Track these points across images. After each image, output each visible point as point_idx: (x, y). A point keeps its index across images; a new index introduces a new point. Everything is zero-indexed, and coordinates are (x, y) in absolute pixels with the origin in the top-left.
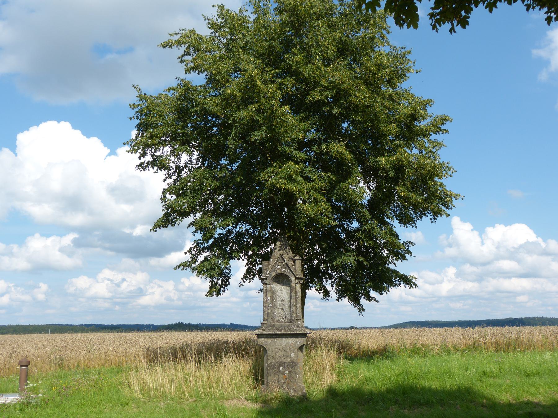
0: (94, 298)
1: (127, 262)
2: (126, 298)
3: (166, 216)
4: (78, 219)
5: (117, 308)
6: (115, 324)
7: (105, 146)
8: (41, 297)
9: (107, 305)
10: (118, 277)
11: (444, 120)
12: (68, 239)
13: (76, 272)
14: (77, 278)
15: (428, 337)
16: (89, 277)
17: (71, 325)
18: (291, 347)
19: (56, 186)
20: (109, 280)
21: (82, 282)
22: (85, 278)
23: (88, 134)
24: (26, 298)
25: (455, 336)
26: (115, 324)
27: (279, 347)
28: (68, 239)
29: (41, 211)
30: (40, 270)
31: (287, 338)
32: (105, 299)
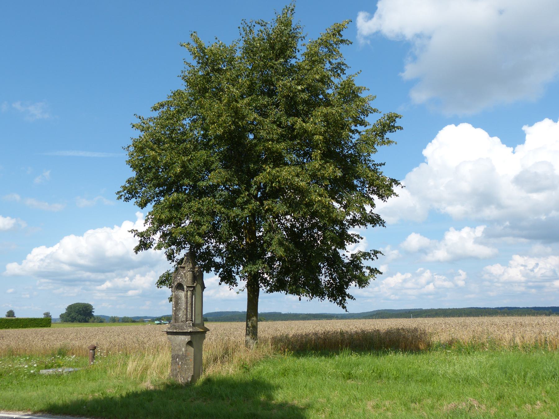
0: (510, 283)
1: (538, 247)
2: (539, 282)
3: (140, 245)
4: (490, 212)
5: (533, 291)
6: (547, 306)
7: (503, 143)
8: (461, 283)
9: (522, 289)
10: (531, 263)
11: (392, 118)
12: (480, 230)
13: (491, 260)
14: (492, 265)
15: (503, 329)
16: (502, 265)
17: (485, 308)
19: (465, 187)
20: (522, 265)
21: (496, 269)
22: (499, 265)
23: (491, 135)
24: (448, 284)
25: (531, 329)
26: (424, 308)
28: (480, 230)
29: (456, 210)
30: (459, 260)
32: (519, 283)
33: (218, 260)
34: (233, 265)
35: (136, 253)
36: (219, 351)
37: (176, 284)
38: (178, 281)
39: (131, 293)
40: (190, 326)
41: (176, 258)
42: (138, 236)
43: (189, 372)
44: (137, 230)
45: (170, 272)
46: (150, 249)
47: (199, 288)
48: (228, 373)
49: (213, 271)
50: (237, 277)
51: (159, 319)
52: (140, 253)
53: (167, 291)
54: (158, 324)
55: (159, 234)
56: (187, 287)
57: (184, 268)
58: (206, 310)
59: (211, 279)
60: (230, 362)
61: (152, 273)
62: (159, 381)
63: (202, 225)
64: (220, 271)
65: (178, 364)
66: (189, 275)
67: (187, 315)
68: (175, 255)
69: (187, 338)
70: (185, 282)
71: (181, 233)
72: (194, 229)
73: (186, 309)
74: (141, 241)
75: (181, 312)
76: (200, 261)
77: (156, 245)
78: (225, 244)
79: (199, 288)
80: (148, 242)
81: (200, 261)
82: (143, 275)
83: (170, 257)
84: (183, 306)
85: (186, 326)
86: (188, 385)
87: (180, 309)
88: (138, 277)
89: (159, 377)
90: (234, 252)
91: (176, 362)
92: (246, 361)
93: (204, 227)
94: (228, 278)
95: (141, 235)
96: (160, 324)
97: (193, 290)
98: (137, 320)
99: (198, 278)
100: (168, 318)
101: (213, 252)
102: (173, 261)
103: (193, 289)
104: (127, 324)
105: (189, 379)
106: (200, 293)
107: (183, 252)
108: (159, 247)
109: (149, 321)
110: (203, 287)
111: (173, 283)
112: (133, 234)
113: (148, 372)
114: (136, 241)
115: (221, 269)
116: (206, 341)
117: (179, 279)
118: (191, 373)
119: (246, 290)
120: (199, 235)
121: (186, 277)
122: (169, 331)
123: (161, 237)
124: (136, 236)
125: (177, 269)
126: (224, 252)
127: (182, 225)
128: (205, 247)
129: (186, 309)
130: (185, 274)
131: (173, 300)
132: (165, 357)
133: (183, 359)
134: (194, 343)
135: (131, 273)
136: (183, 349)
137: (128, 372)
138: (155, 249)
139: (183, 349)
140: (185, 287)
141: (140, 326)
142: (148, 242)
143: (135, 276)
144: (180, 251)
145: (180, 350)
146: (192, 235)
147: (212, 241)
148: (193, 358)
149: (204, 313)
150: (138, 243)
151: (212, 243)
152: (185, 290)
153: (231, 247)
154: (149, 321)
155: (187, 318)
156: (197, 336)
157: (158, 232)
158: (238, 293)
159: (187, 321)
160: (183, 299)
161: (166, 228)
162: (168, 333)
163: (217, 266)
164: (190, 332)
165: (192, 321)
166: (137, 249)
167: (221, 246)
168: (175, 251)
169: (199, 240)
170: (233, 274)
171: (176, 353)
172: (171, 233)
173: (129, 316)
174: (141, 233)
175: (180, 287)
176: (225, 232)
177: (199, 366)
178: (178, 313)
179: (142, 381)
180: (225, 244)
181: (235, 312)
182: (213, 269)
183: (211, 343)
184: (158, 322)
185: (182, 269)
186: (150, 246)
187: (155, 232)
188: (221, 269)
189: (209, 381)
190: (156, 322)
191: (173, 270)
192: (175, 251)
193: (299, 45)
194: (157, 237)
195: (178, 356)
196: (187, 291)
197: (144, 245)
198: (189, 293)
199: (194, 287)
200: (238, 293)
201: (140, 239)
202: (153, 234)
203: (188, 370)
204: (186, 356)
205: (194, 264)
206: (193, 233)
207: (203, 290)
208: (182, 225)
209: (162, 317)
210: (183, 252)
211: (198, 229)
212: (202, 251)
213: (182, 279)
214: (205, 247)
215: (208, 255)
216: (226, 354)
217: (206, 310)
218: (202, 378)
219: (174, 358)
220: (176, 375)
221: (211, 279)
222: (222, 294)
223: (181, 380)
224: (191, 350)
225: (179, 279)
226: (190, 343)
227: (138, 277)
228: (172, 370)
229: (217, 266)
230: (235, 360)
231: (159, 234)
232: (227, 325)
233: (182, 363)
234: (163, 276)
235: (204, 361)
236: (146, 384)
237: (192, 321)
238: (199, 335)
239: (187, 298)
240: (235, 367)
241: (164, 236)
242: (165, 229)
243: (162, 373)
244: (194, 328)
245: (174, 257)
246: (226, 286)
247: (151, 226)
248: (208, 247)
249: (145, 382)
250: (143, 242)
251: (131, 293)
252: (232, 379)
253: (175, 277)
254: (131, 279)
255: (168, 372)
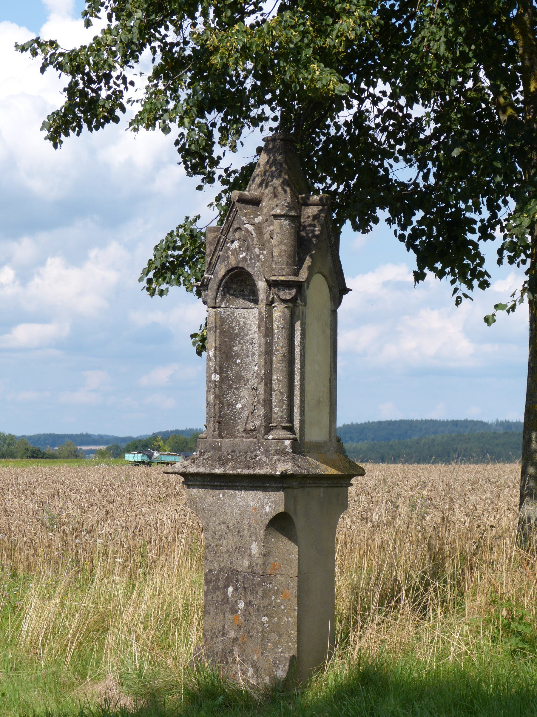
3: (70, 108)
18: (252, 521)
27: (228, 518)
31: (245, 488)
33: (403, 172)
34: (474, 191)
35: (55, 139)
36: (408, 559)
37: (221, 270)
38: (233, 262)
39: (23, 334)
40: (282, 452)
41: (223, 164)
42: (60, 67)
43: (278, 643)
44: (53, 43)
45: (200, 225)
46: (111, 126)
47: (318, 290)
48: (445, 653)
49: (382, 222)
50: (488, 249)
51: (144, 445)
52: (70, 141)
53: (186, 310)
54: (137, 463)
55: (148, 59)
56: (271, 284)
57: (256, 202)
58: (351, 411)
59: (375, 259)
60: (454, 605)
61: (114, 249)
62: (155, 674)
63: (336, 17)
64: (415, 219)
65: (234, 611)
66: (279, 234)
67: (268, 403)
68: (217, 150)
69: (271, 503)
70: (259, 276)
71: (245, 52)
72: (304, 34)
73: (267, 379)
74: (71, 90)
75: (245, 392)
76: (329, 180)
77: (137, 108)
78: (435, 104)
79: (318, 290)
80: (104, 94)
81: (329, 180)
82: (76, 258)
83: (197, 158)
84: (253, 367)
85: (267, 452)
86: (283, 691)
87: (239, 378)
88: (54, 266)
89: (154, 663)
90: (471, 138)
91: (226, 601)
92: (518, 604)
93: (346, 24)
94: (445, 251)
95: (73, 63)
96: (149, 464)
97: (293, 300)
98: (48, 449)
99: (316, 260)
100: (182, 443)
101: (382, 137)
102: (210, 179)
103: (295, 294)
104: (11, 462)
105: (281, 673)
106: (327, 312)
107: (252, 138)
108: (150, 117)
109: (102, 454)
110: (339, 289)
111: (212, 267)
112: (40, 59)
113: (110, 640)
114: (53, 91)
115: (419, 214)
116: (347, 523)
117: (234, 253)
118: (287, 649)
119: (524, 310)
120: (325, 56)
121: (266, 243)
122: (193, 469)
123: (157, 74)
124: (50, 69)
125: (228, 213)
126: (428, 139)
127: (249, 21)
128: (345, 115)
129: (267, 379)
130: (259, 228)
131: (211, 343)
132: (178, 583)
133: (253, 589)
134: (300, 522)
135: (25, 248)
136: (255, 548)
137: (24, 639)
138: (135, 123)
139: (255, 548)
140: (261, 285)
141: (64, 470)
142: (104, 94)
143: (42, 263)
144: (238, 133)
145: (241, 550)
146: (291, 54)
147: (376, 91)
148: (294, 584)
149: (340, 423)
150: (60, 101)
151: (376, 101)
152: (262, 296)
153: (463, 117)
154: (102, 454)
155: (268, 417)
156: (314, 485)
157: (147, 52)
158: (489, 320)
159: (268, 429)
160: (255, 336)
161: (182, 34)
162: (191, 480)
163: (402, 201)
164: (284, 476)
165: (291, 429)
166: (60, 126)
167: (418, 111)
168: (217, 135)
169: (322, 77)
170: (469, 236)
171: (225, 562)
172: (203, 55)
173: (18, 432)
174: (73, 56)
175: (238, 284)
176: (434, 46)
177: (319, 623)
178: (230, 397)
179: (83, 676)
180: (435, 104)
181: (466, 424)
182: (383, 214)
183: (380, 514)
184: (139, 457)
185: (249, 208)
186: (111, 111)
187: (130, 54)
188: (419, 214)
189: (371, 680)
190: (129, 457)
191: (209, 218)
192: (217, 135)
193: (364, 464)
194: (138, 78)
195: (232, 576)
196: (270, 304)
197: (85, 110)
198: (279, 311)
199: (299, 286)
200: (489, 320)
201: (67, 79)
202: (125, 62)
203: (274, 637)
204: (265, 577)
205: (300, 189)
206: (298, 50)
207: (337, 301)
208: (249, 21)
209: (155, 437)
210: (252, 138)
211: (322, 32)
212: (333, 131)
213: (248, 249)
214: (345, 115)
215: (358, 153)
216: (434, 577)
217: (351, 411)
218: (338, 669)
219: (214, 583)
220: (227, 653)
221: (375, 259)
222: (409, 344)
223: (245, 677)
224: (287, 550)
225: (236, 252)
226: (281, 524)
227: (54, 266)
228: (208, 636)
229: (402, 201)
230: (475, 603)
231: (148, 59)
232: (435, 472)
233: (248, 604)
234: (170, 243)
235: (342, 604)
236: (99, 688)
237: (291, 429)
238: (320, 492)
239: (268, 332)
240: (475, 630)
241: (171, 67)
242: (172, 37)
243: (165, 646)
244: (300, 460)
245: (215, 163)
246: (438, 286)
247: (115, 23)
248: (360, 117)
249: (97, 679)
250: (83, 94)
251: (23, 334)
252: (463, 676)
253: (220, 244)
254: (24, 276)
255: (189, 643)
